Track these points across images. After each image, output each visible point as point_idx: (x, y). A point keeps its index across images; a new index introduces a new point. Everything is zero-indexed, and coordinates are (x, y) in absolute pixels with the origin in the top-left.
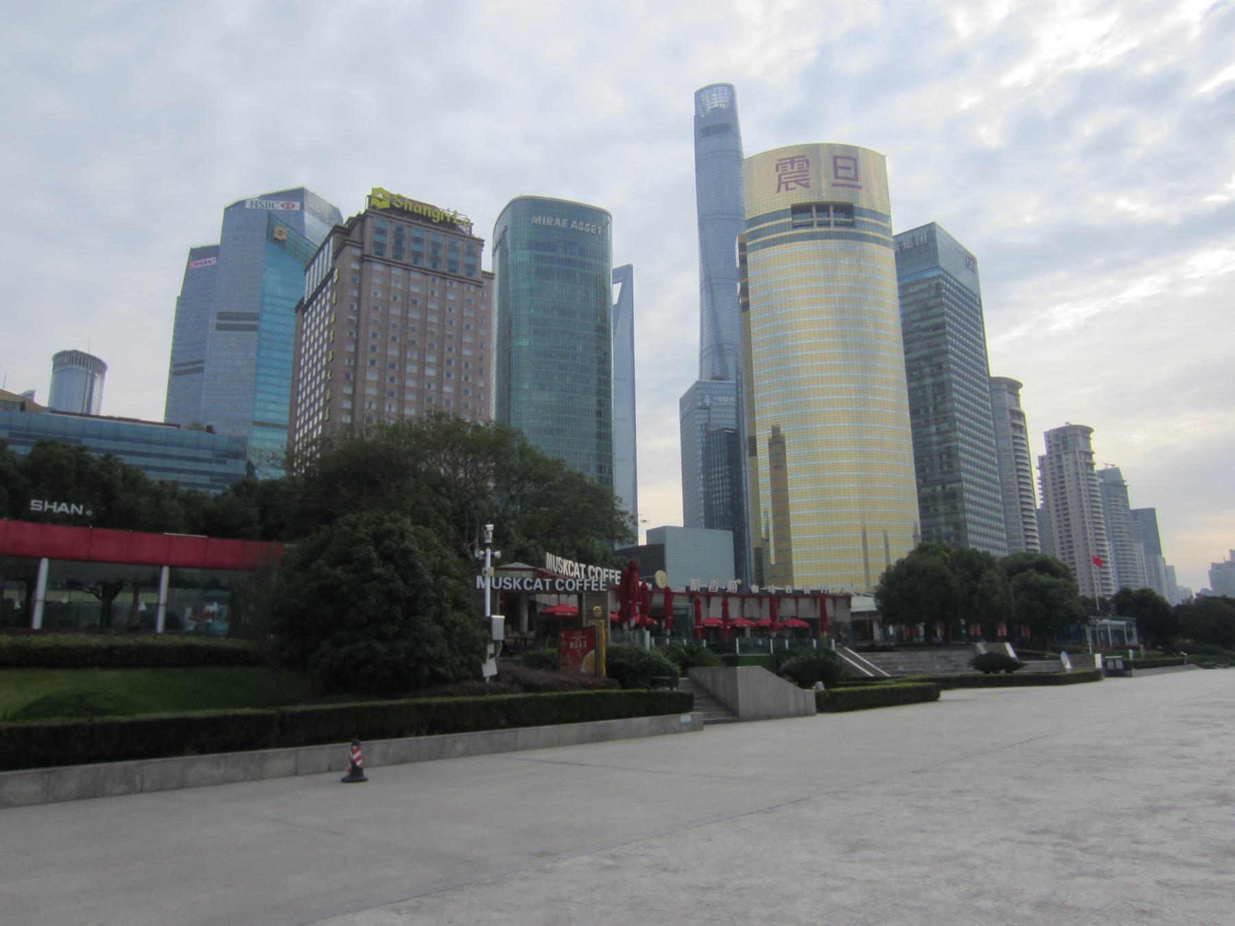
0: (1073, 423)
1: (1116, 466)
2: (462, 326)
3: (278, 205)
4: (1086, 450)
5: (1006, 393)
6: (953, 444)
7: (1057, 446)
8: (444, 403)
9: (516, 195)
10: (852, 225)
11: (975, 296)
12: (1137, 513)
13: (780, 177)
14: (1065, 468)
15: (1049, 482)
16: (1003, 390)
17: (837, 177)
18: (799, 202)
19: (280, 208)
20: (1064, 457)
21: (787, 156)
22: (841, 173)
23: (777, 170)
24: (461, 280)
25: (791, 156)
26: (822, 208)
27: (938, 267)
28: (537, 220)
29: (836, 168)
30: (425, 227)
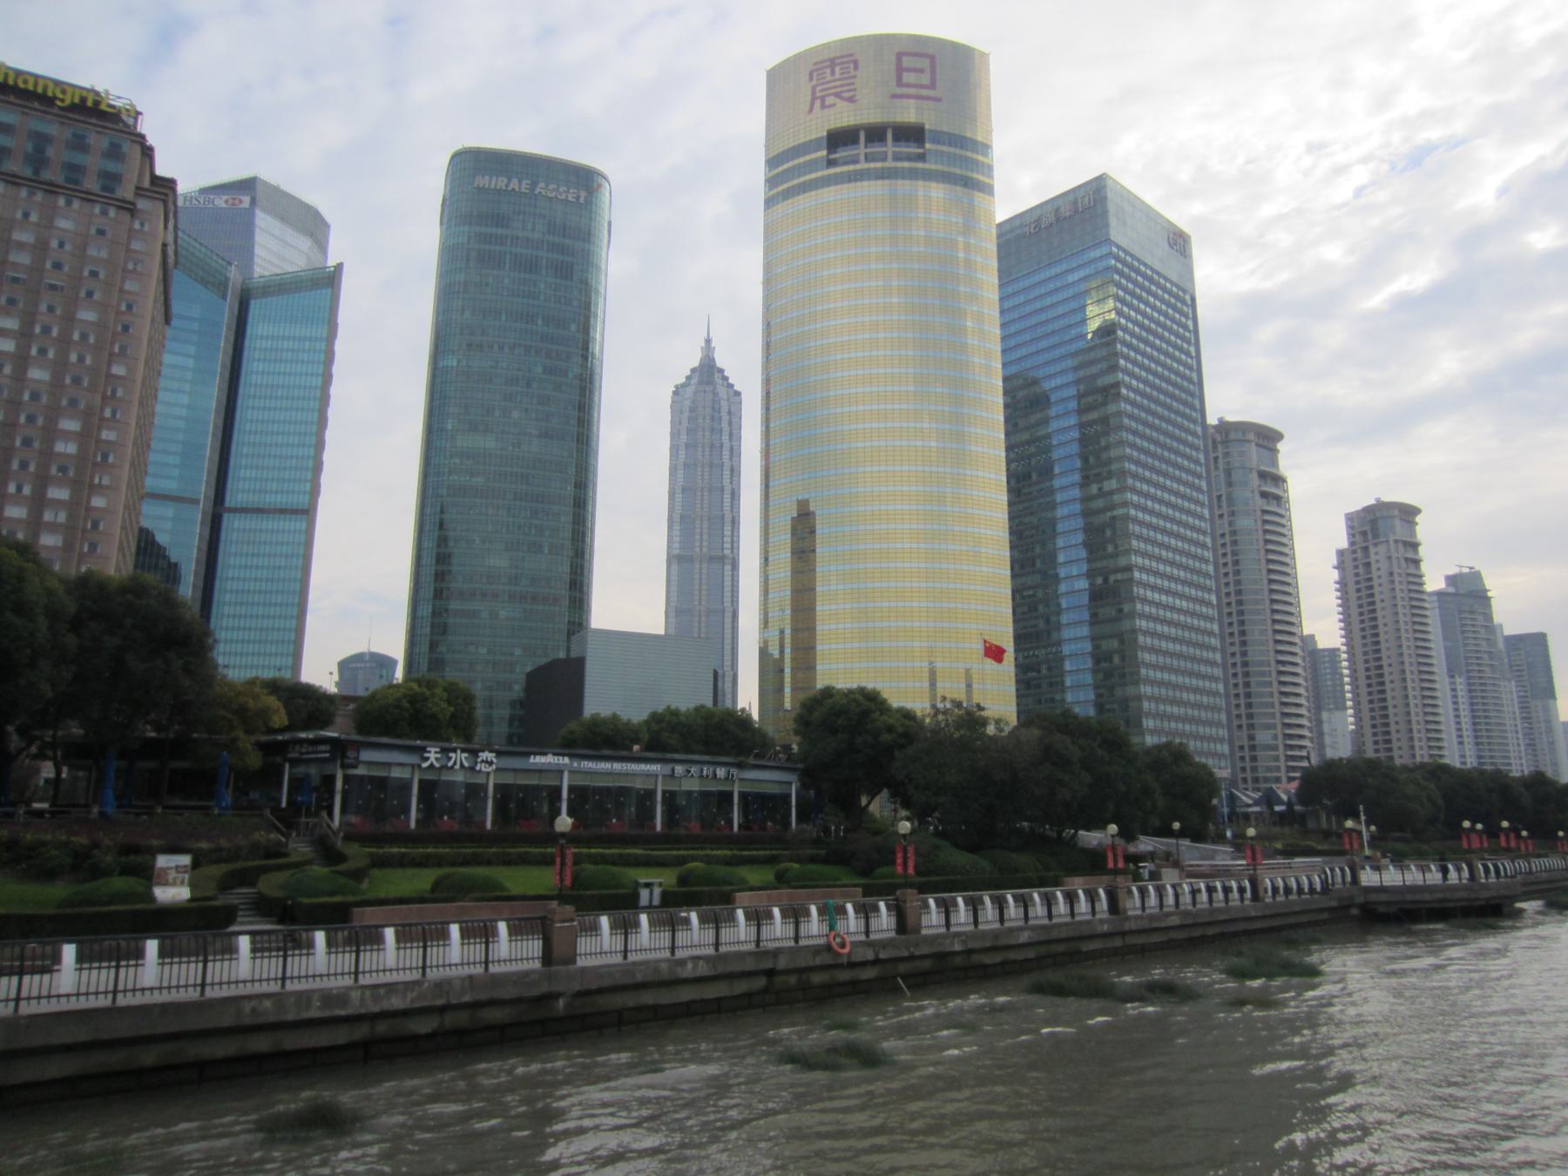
0: (1387, 498)
1: (1477, 568)
2: (81, 271)
3: (220, 202)
4: (1408, 539)
5: (1253, 448)
6: (1119, 512)
7: (1364, 534)
8: (26, 397)
9: (458, 147)
10: (921, 158)
11: (1184, 291)
12: (1517, 642)
13: (814, 88)
14: (1374, 567)
15: (1352, 588)
16: (1248, 441)
17: (900, 83)
18: (845, 124)
19: (224, 205)
20: (1372, 550)
21: (826, 57)
22: (909, 78)
23: (811, 79)
24: (88, 198)
25: (832, 55)
26: (876, 134)
27: (1108, 241)
28: (483, 181)
29: (900, 70)
30: (21, 106)
